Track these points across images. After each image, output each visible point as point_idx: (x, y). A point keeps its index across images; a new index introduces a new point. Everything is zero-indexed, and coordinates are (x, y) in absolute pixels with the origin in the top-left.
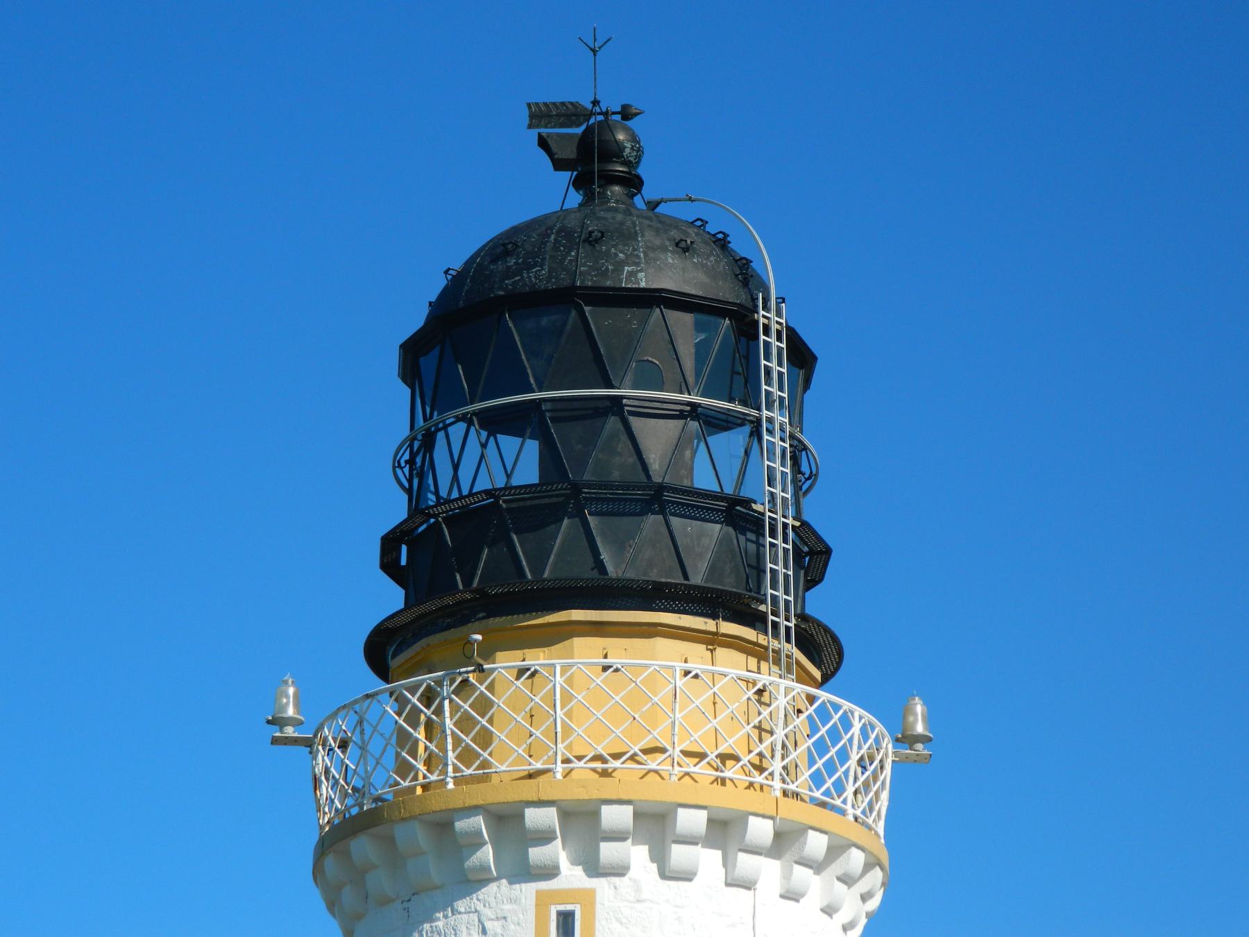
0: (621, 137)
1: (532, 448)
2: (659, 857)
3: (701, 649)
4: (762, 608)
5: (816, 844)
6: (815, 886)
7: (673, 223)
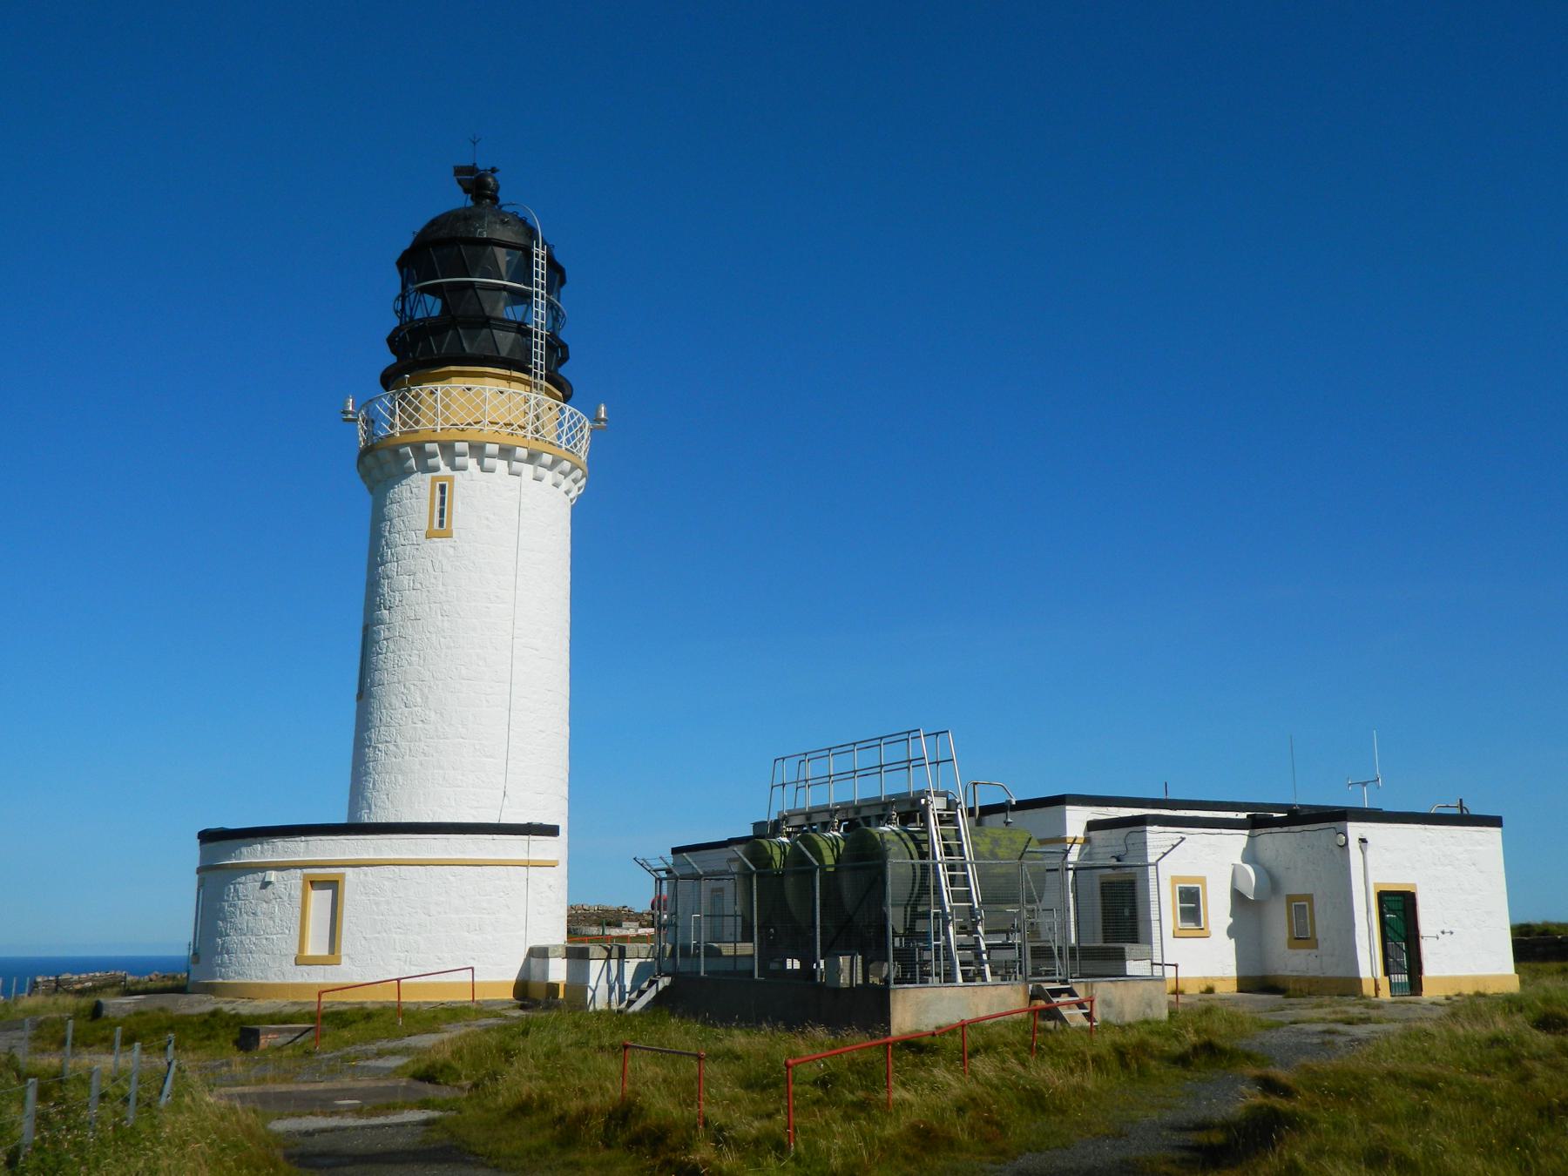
0: (490, 180)
1: (439, 302)
2: (480, 463)
3: (505, 382)
4: (530, 366)
5: (547, 459)
6: (549, 476)
7: (505, 214)
